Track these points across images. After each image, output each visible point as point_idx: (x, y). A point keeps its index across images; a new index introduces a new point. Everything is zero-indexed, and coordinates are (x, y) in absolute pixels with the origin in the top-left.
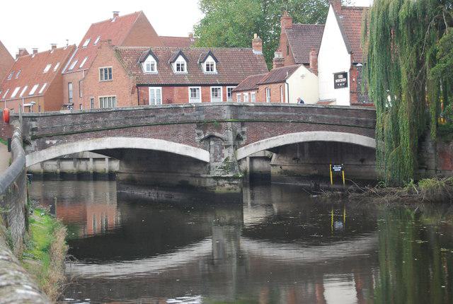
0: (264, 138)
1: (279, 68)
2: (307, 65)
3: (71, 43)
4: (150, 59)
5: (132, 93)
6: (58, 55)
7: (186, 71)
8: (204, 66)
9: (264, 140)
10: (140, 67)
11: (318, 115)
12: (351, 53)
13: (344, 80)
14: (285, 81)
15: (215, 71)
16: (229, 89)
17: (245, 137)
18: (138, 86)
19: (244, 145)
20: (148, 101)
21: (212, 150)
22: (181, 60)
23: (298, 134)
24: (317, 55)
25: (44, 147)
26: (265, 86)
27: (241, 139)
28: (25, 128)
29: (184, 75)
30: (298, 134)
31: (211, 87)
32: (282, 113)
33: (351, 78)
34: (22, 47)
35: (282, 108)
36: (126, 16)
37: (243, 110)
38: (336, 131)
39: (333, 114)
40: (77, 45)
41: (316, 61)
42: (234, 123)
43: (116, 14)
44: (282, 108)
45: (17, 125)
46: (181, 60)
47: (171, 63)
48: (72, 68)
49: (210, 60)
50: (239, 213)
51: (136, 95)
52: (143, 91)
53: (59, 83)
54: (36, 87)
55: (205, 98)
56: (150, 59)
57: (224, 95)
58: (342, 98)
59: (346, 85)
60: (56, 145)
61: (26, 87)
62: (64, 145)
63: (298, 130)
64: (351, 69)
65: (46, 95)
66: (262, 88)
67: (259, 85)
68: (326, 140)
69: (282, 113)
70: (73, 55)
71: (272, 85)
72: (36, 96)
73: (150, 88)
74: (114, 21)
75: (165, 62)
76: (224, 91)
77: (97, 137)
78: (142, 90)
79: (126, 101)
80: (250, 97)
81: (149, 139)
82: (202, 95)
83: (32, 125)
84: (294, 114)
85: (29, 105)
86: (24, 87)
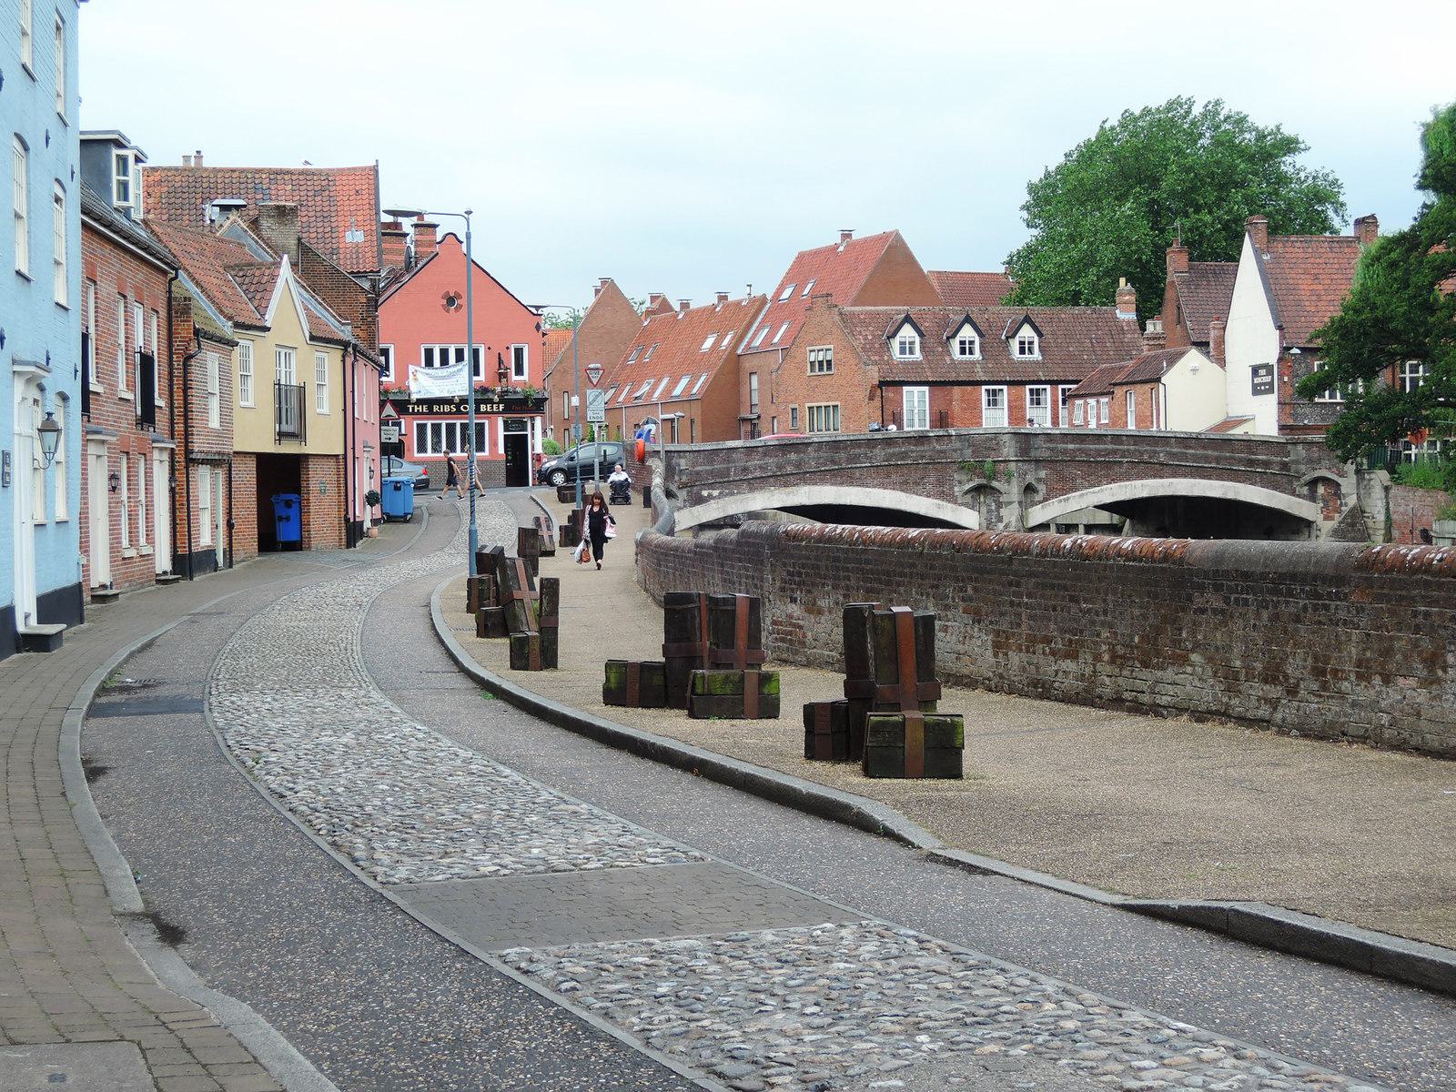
0: (1077, 490)
1: (1152, 353)
2: (1202, 345)
3: (757, 293)
4: (907, 332)
5: (871, 398)
7: (977, 355)
8: (1015, 345)
10: (886, 346)
11: (1175, 450)
12: (1280, 328)
13: (1268, 379)
14: (1158, 380)
15: (1037, 355)
16: (1063, 390)
17: (1042, 488)
18: (882, 384)
20: (901, 414)
21: (984, 509)
22: (967, 332)
24: (1224, 328)
25: (698, 500)
26: (1125, 388)
28: (670, 472)
29: (973, 363)
30: (1138, 483)
31: (1028, 387)
32: (1110, 447)
33: (1281, 376)
34: (656, 290)
36: (865, 241)
37: (1040, 442)
38: (1210, 479)
39: (1204, 448)
40: (769, 297)
41: (1221, 342)
42: (1020, 464)
43: (846, 235)
45: (657, 466)
46: (967, 332)
47: (948, 338)
48: (757, 342)
51: (877, 402)
53: (733, 370)
54: (684, 382)
55: (1016, 413)
56: (907, 332)
57: (1055, 402)
58: (1263, 418)
59: (1271, 391)
60: (719, 497)
62: (732, 498)
63: (1139, 477)
64: (1280, 360)
65: (705, 399)
66: (1119, 391)
67: (1115, 385)
68: (1190, 494)
69: (1110, 447)
71: (1139, 386)
72: (687, 401)
75: (936, 337)
76: (1054, 395)
77: (786, 485)
78: (889, 393)
79: (857, 422)
80: (1099, 409)
82: (1009, 401)
85: (672, 416)
86: (660, 380)
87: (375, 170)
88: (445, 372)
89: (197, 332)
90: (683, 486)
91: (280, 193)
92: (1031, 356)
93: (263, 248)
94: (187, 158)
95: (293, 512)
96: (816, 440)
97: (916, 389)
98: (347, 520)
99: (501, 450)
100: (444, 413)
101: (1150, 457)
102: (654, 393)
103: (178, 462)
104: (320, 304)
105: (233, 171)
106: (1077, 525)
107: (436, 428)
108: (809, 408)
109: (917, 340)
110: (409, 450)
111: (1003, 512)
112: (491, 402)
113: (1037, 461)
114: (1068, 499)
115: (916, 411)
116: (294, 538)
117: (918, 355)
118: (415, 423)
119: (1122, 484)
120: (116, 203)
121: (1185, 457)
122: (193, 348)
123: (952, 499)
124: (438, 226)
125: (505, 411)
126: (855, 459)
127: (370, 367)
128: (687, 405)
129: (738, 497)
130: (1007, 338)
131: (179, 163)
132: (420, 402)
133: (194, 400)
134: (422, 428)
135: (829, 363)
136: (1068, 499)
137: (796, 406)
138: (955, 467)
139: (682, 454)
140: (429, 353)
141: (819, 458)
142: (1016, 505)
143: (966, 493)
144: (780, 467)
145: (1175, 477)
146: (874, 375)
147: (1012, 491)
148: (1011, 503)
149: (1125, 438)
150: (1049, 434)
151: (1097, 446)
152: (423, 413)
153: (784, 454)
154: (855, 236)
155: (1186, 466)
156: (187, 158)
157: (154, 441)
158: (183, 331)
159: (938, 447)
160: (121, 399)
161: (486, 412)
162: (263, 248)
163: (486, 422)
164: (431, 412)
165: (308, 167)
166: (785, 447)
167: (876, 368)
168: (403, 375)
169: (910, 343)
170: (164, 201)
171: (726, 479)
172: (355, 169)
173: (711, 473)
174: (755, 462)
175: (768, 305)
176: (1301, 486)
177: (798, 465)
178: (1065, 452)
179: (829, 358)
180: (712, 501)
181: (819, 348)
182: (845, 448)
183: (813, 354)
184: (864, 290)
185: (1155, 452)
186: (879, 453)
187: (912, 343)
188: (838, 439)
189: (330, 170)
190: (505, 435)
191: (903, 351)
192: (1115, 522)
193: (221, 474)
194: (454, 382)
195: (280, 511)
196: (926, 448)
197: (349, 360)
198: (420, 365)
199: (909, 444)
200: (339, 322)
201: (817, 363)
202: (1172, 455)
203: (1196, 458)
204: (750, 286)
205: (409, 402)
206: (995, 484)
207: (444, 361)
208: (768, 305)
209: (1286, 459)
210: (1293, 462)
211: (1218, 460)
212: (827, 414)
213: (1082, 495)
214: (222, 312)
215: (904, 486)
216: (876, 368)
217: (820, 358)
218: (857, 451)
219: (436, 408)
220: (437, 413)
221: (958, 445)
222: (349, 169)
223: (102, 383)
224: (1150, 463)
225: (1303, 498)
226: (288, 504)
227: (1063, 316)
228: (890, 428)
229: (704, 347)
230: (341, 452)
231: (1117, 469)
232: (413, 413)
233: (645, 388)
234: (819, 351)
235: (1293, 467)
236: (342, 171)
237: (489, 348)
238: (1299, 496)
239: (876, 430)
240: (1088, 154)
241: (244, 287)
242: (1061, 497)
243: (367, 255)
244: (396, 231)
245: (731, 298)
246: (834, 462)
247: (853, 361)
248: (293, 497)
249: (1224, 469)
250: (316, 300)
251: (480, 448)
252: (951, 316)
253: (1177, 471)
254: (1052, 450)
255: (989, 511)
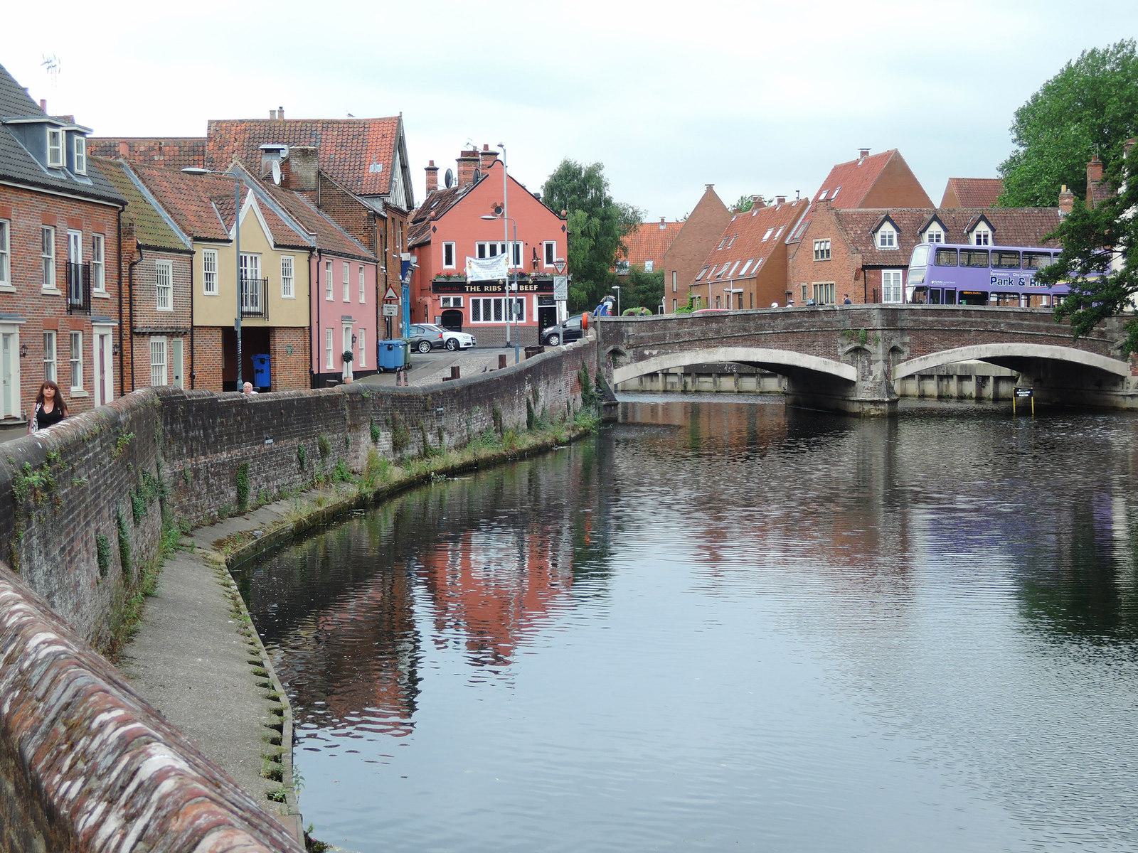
0: (934, 351)
3: (802, 197)
4: (887, 228)
5: (857, 279)
6: (789, 213)
8: (973, 237)
9: (935, 354)
10: (871, 239)
17: (907, 350)
18: (865, 268)
19: (905, 361)
21: (860, 365)
23: (983, 346)
25: (641, 358)
27: (901, 352)
32: (961, 319)
35: (961, 312)
37: (905, 315)
38: (1041, 343)
40: (811, 200)
43: (864, 153)
44: (961, 312)
47: (921, 233)
49: (982, 228)
50: (278, 334)
51: (861, 282)
52: (872, 276)
53: (780, 258)
56: (887, 228)
60: (658, 355)
61: (738, 263)
63: (984, 342)
65: (760, 277)
69: (961, 319)
70: (802, 217)
72: (747, 279)
73: (884, 271)
74: (860, 163)
77: (708, 347)
78: (871, 275)
81: (775, 351)
83: (627, 332)
84: (979, 320)
86: (734, 263)
87: (399, 120)
88: (481, 261)
89: (139, 247)
90: (630, 347)
91: (328, 137)
92: (890, 246)
93: (256, 183)
94: (272, 112)
95: (265, 367)
96: (732, 313)
97: (892, 272)
98: (311, 372)
99: (536, 318)
100: (492, 292)
101: (993, 327)
102: (729, 272)
103: (125, 334)
104: (295, 221)
105: (297, 122)
106: (989, 377)
107: (487, 303)
108: (815, 286)
109: (895, 234)
110: (466, 319)
111: (873, 367)
112: (526, 283)
113: (902, 330)
114: (927, 358)
115: (892, 289)
116: (266, 385)
117: (895, 246)
118: (471, 299)
119: (970, 347)
120: (49, 164)
121: (1020, 326)
122: (136, 257)
123: (836, 357)
124: (498, 154)
125: (538, 290)
126: (761, 327)
127: (136, 277)
128: (747, 282)
129: (672, 355)
130: (968, 232)
131: (267, 116)
132: (474, 284)
133: (137, 293)
134: (476, 303)
135: (828, 251)
136: (927, 358)
137: (805, 284)
138: (838, 334)
139: (630, 324)
140: (482, 248)
141: (734, 327)
142: (881, 363)
143: (847, 353)
144: (704, 333)
145: (1013, 342)
146: (858, 261)
147: (878, 352)
148: (877, 361)
149: (973, 312)
150: (913, 309)
151: (951, 318)
152: (477, 292)
153: (707, 324)
154: (871, 154)
155: (1021, 333)
156: (272, 112)
157: (93, 321)
158: (129, 246)
159: (826, 319)
160: (43, 295)
161: (524, 291)
162: (256, 183)
163: (525, 298)
164: (482, 291)
165: (351, 118)
166: (707, 319)
167: (860, 256)
168: (462, 264)
169: (889, 237)
170: (245, 144)
171: (663, 342)
172: (384, 119)
173: (652, 338)
174: (685, 329)
175: (810, 206)
176: (1115, 349)
177: (718, 332)
178: (925, 323)
179: (827, 248)
180: (652, 358)
181: (821, 240)
182: (754, 319)
183: (817, 245)
184: (869, 195)
185: (997, 323)
186: (780, 324)
187: (891, 237)
188: (748, 313)
189: (366, 120)
190: (539, 308)
191: (883, 243)
192: (1014, 375)
193: (182, 343)
194: (498, 268)
195: (257, 365)
196: (817, 319)
197: (314, 261)
198: (475, 258)
199: (803, 316)
200: (308, 234)
201: (825, 252)
202: (1012, 326)
203: (1030, 328)
204: (798, 191)
205: (465, 284)
206: (866, 347)
207: (493, 252)
208: (810, 206)
209: (1103, 329)
210: (1109, 331)
211: (1047, 329)
212: (827, 291)
213: (938, 356)
214: (184, 231)
215: (799, 348)
216: (860, 256)
217: (822, 248)
218: (763, 322)
219: (486, 288)
220: (487, 292)
221: (841, 317)
222: (380, 119)
223: (15, 285)
224: (992, 331)
225: (1116, 358)
226: (262, 362)
227: (1015, 215)
228: (772, 305)
229: (764, 238)
230: (307, 324)
231: (966, 336)
232: (469, 292)
233: (725, 268)
234: (821, 242)
235: (1109, 335)
236: (374, 121)
237: (527, 244)
238: (1113, 357)
239: (811, 305)
240: (1052, 90)
241: (221, 211)
242: (922, 357)
243: (383, 182)
244: (474, 158)
245: (787, 201)
246: (745, 330)
247: (843, 251)
248: (265, 356)
249: (1052, 336)
250: (292, 218)
251: (520, 317)
252: (925, 215)
253: (1013, 338)
254: (915, 321)
255: (864, 367)
